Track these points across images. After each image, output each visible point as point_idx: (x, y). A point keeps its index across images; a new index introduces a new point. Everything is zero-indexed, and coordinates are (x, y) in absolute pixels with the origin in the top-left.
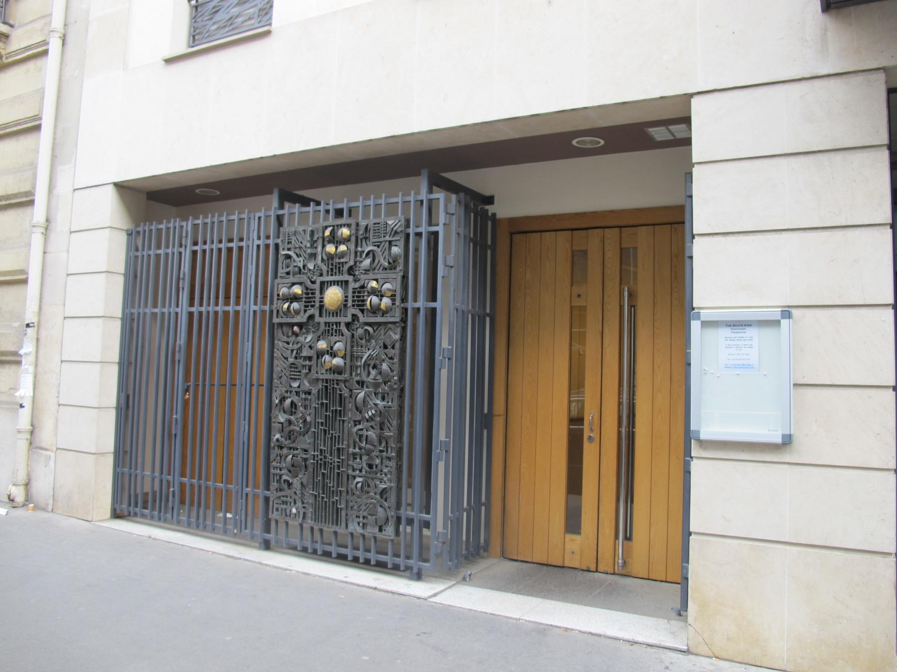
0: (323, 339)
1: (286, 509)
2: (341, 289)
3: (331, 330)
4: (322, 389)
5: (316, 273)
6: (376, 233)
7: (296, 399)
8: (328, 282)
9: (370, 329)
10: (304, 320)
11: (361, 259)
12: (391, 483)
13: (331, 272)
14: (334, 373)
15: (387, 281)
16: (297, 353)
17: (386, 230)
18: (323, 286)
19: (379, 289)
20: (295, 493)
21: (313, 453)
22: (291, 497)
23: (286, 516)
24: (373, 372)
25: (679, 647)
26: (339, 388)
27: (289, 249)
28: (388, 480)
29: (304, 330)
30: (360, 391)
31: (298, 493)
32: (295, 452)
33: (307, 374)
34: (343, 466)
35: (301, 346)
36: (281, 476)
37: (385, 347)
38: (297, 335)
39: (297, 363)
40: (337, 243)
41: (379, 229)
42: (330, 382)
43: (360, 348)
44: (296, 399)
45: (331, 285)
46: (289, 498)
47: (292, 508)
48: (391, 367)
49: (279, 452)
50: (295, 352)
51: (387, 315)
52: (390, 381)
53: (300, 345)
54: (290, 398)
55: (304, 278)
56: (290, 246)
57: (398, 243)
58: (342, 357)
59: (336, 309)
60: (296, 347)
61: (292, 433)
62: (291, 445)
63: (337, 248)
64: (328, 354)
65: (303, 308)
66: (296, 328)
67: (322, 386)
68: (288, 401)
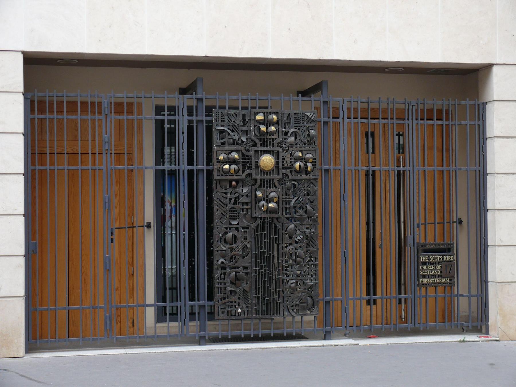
0: (259, 191)
1: (231, 311)
2: (273, 157)
3: (266, 184)
4: (261, 224)
5: (248, 145)
6: (296, 120)
7: (236, 233)
8: (261, 151)
9: (296, 183)
10: (243, 176)
11: (286, 137)
12: (316, 281)
13: (263, 144)
14: (270, 214)
15: (309, 152)
16: (235, 201)
17: (304, 119)
18: (276, 155)
19: (303, 158)
20: (239, 298)
21: (254, 268)
22: (235, 302)
23: (232, 315)
24: (301, 211)
25: (261, 347)
26: (274, 223)
27: (223, 126)
28: (314, 279)
29: (240, 184)
30: (290, 224)
31: (241, 298)
32: (237, 270)
33: (245, 215)
34: (280, 274)
35: (239, 196)
36: (225, 288)
37: (308, 194)
38: (235, 187)
39: (236, 208)
40: (267, 125)
41: (299, 118)
42: (267, 219)
43: (288, 196)
44: (236, 233)
45: (264, 154)
46: (234, 303)
47: (237, 309)
48: (313, 208)
49: (223, 271)
50: (233, 200)
51: (310, 174)
52: (313, 216)
53: (238, 194)
54: (230, 232)
55: (240, 148)
56: (223, 123)
57: (313, 128)
58: (276, 202)
59: (270, 170)
60: (234, 196)
61: (234, 257)
62: (234, 266)
63: (267, 128)
64: (264, 200)
65: (241, 169)
66: (234, 183)
67: (261, 222)
68: (230, 235)
